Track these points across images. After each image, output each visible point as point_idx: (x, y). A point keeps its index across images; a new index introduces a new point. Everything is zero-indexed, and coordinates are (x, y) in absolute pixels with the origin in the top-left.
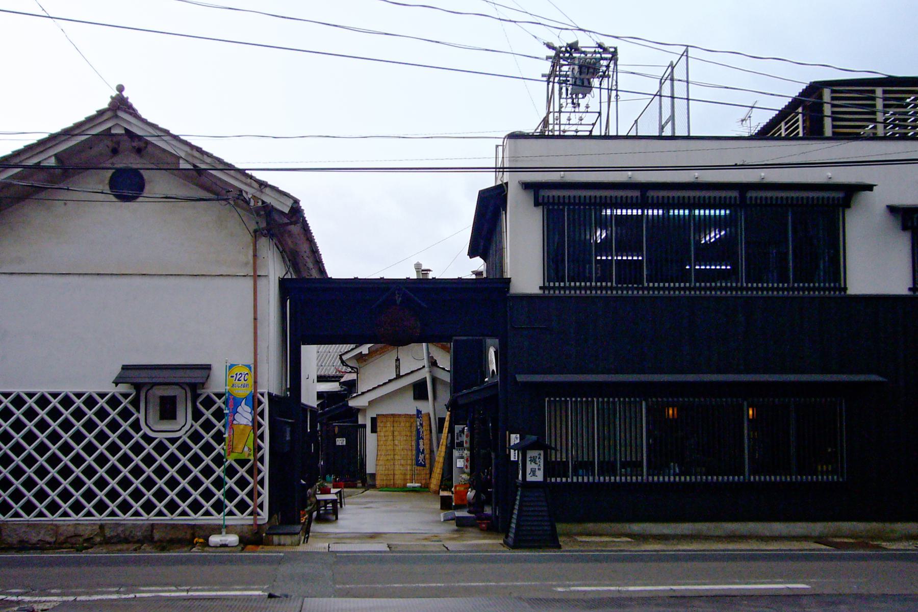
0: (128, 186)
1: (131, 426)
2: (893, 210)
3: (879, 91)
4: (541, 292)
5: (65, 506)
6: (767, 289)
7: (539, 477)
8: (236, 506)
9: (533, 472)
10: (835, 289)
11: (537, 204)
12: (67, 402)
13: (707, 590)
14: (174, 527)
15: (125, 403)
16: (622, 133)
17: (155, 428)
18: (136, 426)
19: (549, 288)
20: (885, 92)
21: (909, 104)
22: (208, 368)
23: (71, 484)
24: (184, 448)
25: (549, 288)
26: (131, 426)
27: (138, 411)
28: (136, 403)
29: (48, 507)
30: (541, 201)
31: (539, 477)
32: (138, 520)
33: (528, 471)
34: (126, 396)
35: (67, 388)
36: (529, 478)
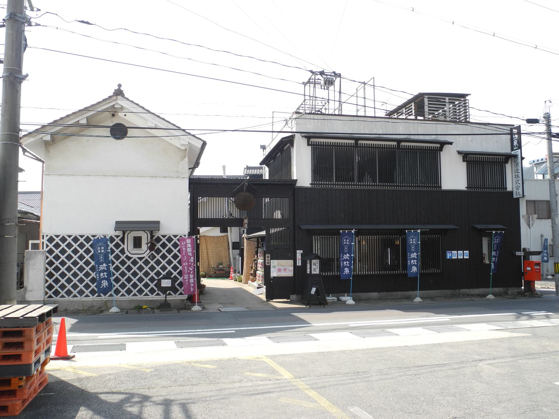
0: (119, 132)
1: (120, 251)
2: (459, 153)
3: (447, 98)
4: (310, 186)
5: (75, 292)
6: (363, 185)
7: (317, 272)
8: (149, 291)
9: (315, 269)
10: (436, 187)
11: (308, 145)
12: (63, 240)
13: (320, 326)
14: (131, 301)
15: (117, 240)
16: (330, 113)
17: (132, 252)
18: (122, 251)
19: (314, 184)
20: (449, 99)
21: (457, 104)
22: (158, 223)
23: (66, 281)
24: (146, 263)
25: (314, 184)
26: (120, 251)
27: (124, 244)
28: (122, 240)
29: (78, 292)
30: (310, 143)
31: (317, 272)
32: (123, 298)
33: (313, 269)
34: (117, 237)
35: (76, 232)
36: (313, 273)
